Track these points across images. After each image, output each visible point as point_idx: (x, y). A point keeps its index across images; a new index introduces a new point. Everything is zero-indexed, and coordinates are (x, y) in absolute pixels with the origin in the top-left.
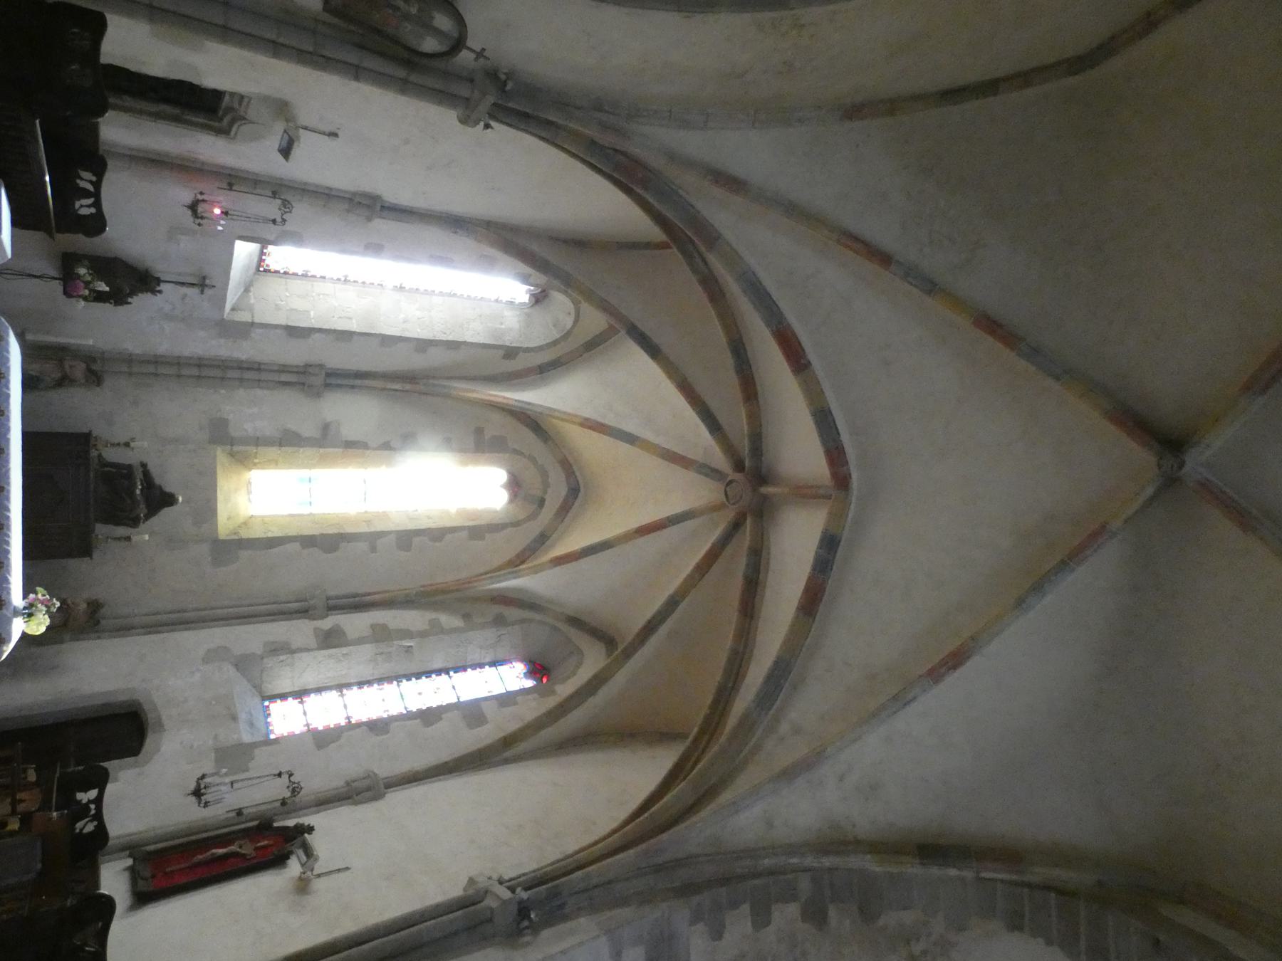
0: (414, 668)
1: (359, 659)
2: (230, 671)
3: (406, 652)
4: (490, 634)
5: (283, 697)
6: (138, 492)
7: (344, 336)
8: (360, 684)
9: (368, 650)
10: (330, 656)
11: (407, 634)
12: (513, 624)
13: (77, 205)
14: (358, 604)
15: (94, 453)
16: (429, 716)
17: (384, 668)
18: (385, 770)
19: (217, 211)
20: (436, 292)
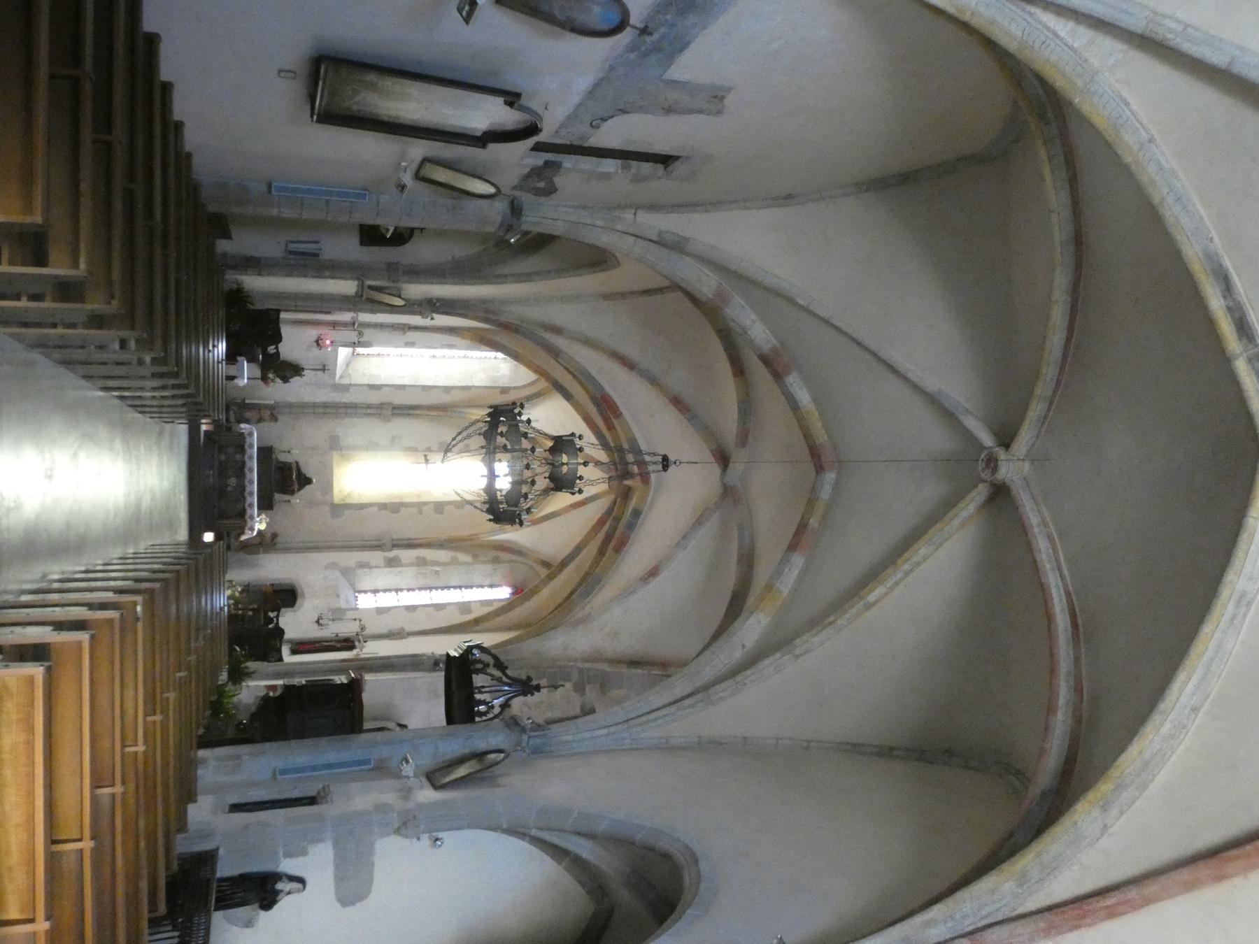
0: (440, 584)
1: (406, 576)
2: (338, 574)
3: (436, 573)
4: (489, 567)
5: (365, 592)
6: (294, 477)
7: (402, 387)
9: (413, 570)
10: (390, 572)
11: (436, 563)
13: (269, 349)
14: (411, 545)
15: (274, 456)
16: (439, 607)
18: (408, 628)
19: (328, 342)
20: (456, 356)
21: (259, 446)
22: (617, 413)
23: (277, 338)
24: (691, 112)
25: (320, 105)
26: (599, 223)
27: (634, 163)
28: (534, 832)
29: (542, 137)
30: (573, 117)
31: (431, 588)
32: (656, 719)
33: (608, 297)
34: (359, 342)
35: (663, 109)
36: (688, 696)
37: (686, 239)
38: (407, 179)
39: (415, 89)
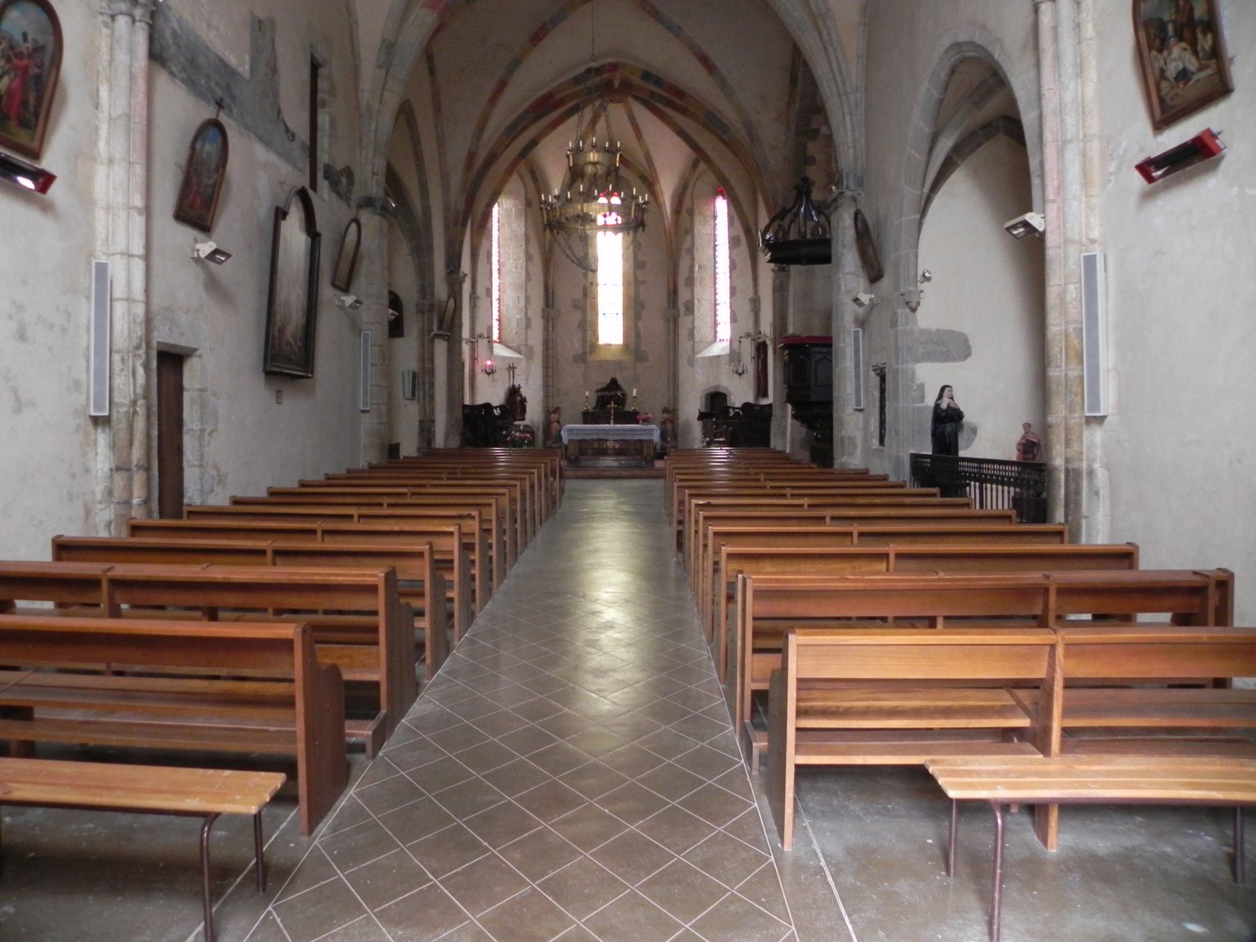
1: (701, 294)
8: (715, 294)
10: (699, 309)
12: (693, 205)
15: (592, 411)
16: (733, 266)
17: (709, 282)
18: (750, 294)
21: (582, 421)
22: (550, 95)
23: (488, 407)
24: (274, 50)
25: (301, 371)
26: (373, 127)
27: (320, 96)
28: (926, 190)
29: (307, 186)
30: (287, 158)
31: (715, 274)
32: (840, 69)
33: (438, 109)
34: (488, 337)
35: (273, 76)
36: (820, 33)
37: (383, 41)
38: (349, 300)
39: (282, 295)
